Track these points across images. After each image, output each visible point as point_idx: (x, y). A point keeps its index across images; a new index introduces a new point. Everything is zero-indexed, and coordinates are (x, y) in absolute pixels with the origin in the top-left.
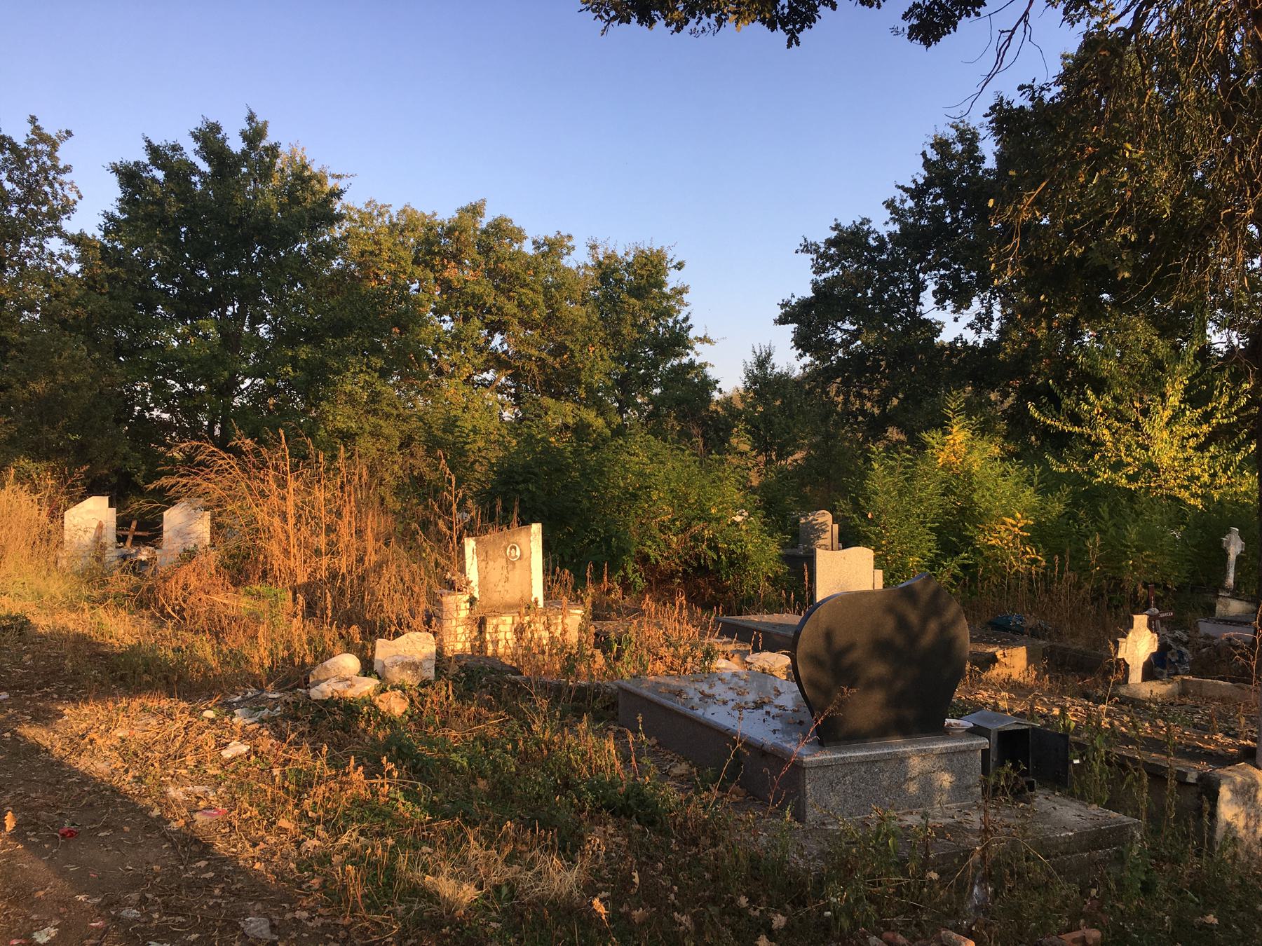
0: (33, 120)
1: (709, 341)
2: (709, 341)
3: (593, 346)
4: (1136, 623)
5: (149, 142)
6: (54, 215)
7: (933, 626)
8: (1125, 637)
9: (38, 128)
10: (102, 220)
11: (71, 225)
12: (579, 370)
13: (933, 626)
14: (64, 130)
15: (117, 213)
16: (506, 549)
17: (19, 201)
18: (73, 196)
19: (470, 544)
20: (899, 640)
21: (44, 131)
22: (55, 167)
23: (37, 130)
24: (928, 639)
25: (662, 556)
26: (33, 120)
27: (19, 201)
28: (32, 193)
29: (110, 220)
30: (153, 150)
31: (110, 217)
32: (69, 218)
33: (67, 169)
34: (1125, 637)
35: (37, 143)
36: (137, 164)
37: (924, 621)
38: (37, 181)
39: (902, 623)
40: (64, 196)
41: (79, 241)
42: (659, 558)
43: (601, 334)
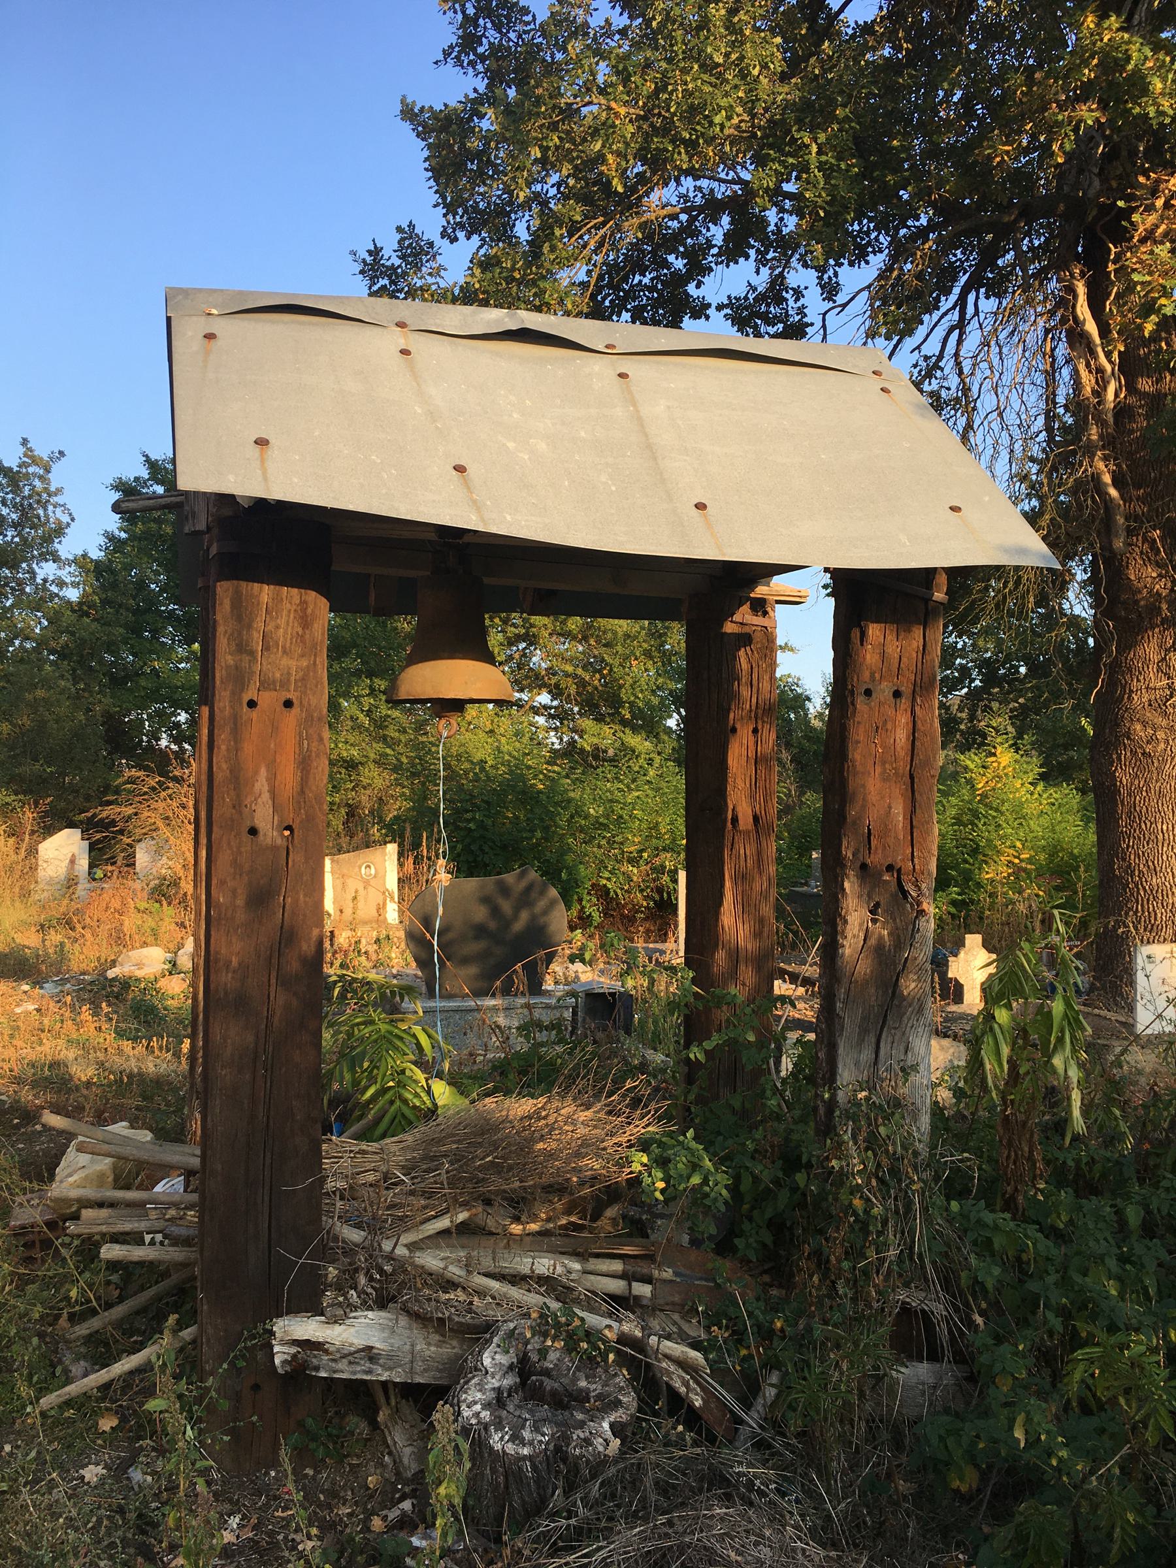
0: (25, 442)
1: (792, 650)
2: (792, 650)
3: (636, 659)
4: (967, 942)
5: (147, 456)
6: (48, 539)
7: (524, 916)
8: (956, 955)
9: (30, 450)
10: (102, 540)
11: (67, 547)
12: (621, 687)
13: (524, 916)
14: (56, 451)
15: (117, 532)
16: (360, 868)
17: (15, 525)
18: (65, 519)
19: (328, 862)
20: (492, 925)
21: (36, 453)
22: (46, 490)
23: (29, 452)
24: (519, 926)
25: (622, 889)
26: (25, 442)
27: (15, 525)
28: (27, 517)
29: (110, 540)
30: (152, 465)
31: (111, 537)
32: (60, 542)
33: (59, 491)
34: (956, 955)
35: (29, 465)
36: (137, 479)
37: (517, 910)
38: (30, 505)
39: (495, 911)
40: (57, 519)
41: (82, 561)
42: (619, 891)
43: (645, 645)
